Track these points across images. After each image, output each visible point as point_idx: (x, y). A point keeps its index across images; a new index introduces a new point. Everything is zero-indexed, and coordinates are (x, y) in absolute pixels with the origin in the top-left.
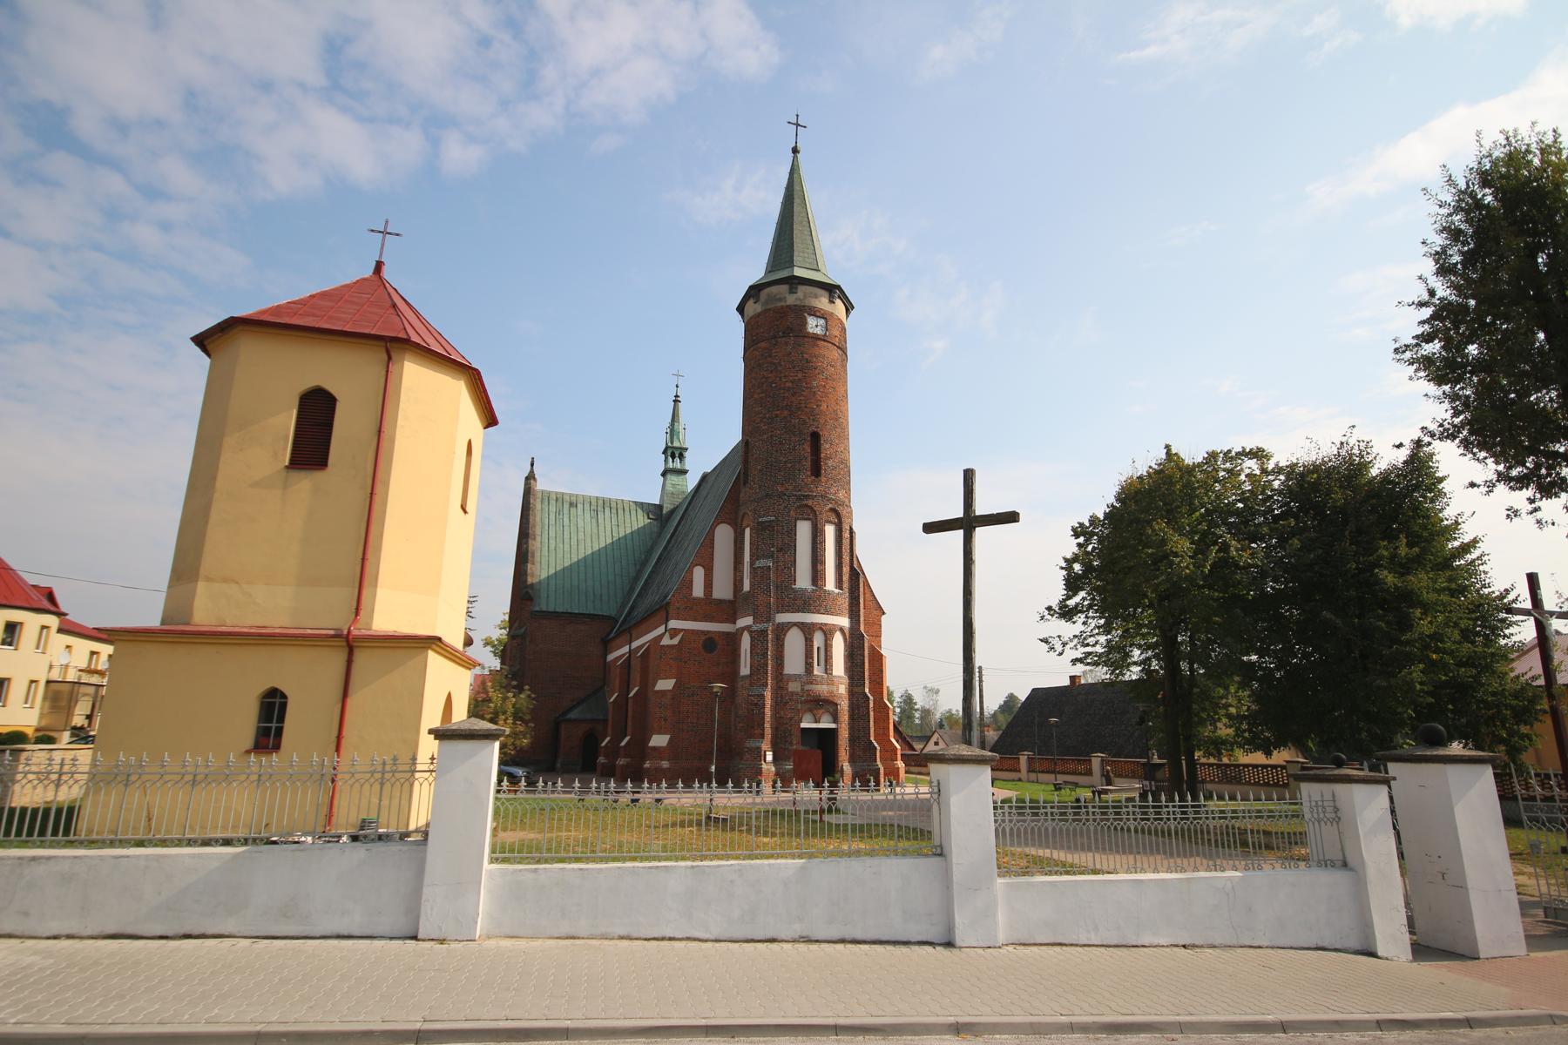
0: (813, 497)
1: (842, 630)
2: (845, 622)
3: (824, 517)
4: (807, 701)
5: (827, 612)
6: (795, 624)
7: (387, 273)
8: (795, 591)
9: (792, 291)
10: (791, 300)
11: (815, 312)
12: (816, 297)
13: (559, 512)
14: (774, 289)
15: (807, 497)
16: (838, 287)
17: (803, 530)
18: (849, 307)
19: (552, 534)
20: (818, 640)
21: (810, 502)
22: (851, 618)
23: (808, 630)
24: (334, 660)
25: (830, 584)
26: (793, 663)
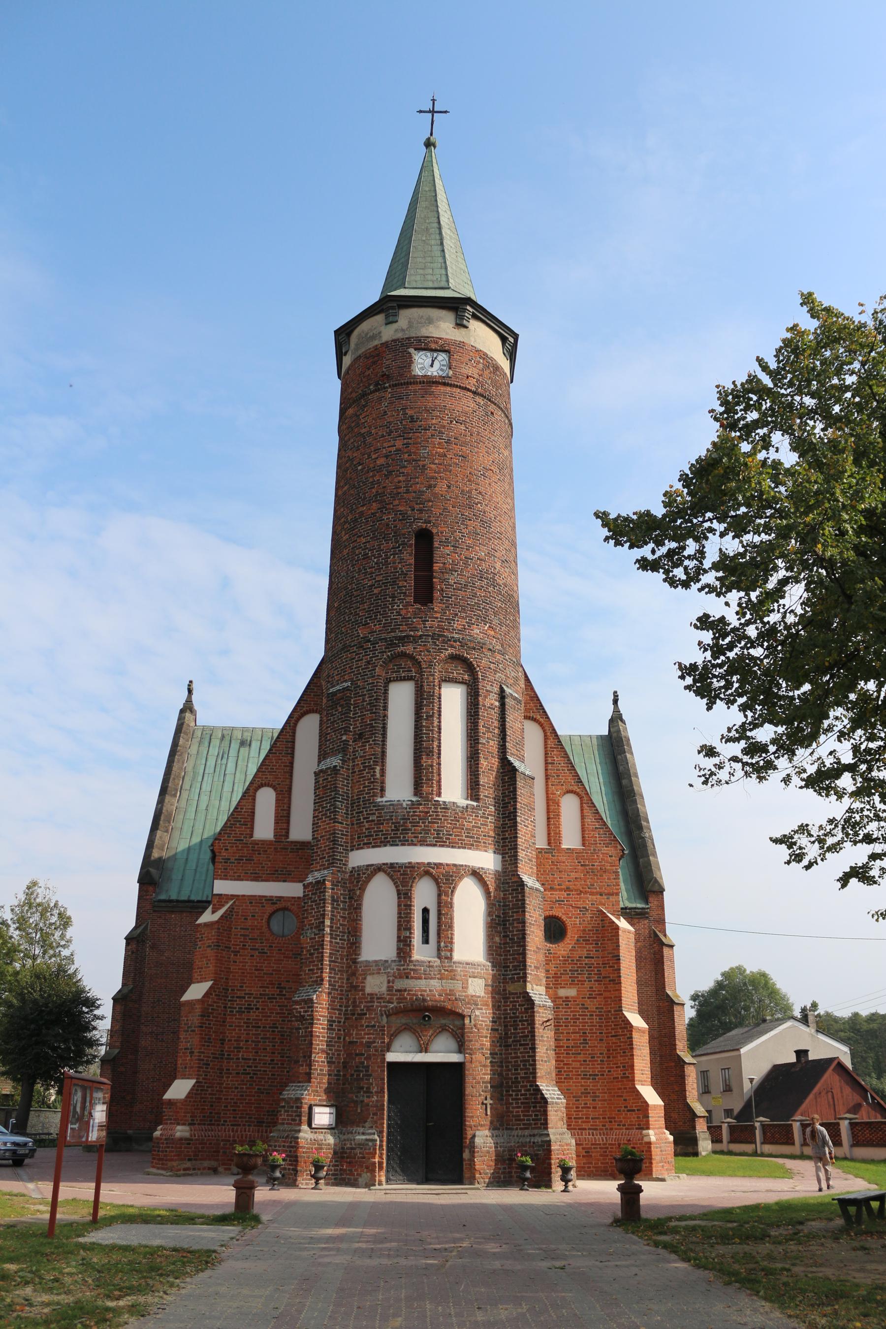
0: (416, 639)
1: (476, 874)
2: (487, 860)
3: (438, 671)
4: (397, 1012)
5: (440, 841)
6: (379, 869)
8: (380, 808)
10: (388, 333)
11: (425, 345)
12: (430, 321)
13: (223, 755)
16: (468, 301)
17: (401, 698)
18: (509, 339)
19: (206, 787)
20: (424, 894)
21: (409, 649)
23: (403, 877)
25: (452, 788)
26: (377, 942)
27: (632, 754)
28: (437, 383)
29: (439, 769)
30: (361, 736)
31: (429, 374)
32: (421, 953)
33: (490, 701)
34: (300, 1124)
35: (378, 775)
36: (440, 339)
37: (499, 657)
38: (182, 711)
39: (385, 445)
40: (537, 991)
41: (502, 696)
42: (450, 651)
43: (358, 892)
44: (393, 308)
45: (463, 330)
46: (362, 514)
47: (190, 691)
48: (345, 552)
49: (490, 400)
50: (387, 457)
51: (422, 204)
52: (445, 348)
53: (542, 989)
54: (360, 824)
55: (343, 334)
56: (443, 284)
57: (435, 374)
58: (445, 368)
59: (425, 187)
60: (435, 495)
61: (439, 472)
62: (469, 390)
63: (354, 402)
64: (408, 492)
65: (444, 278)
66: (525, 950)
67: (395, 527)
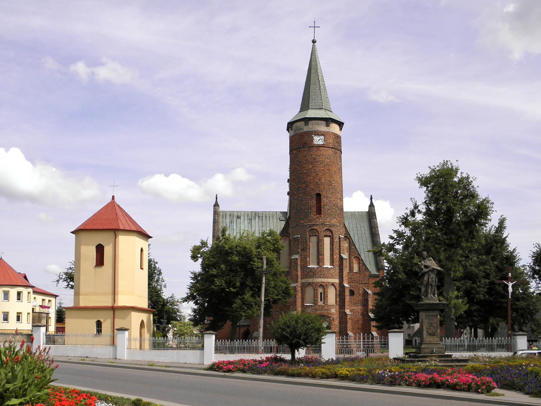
0: (317, 225)
1: (333, 284)
7: (116, 200)
9: (306, 124)
10: (306, 129)
11: (318, 134)
13: (231, 222)
14: (298, 124)
15: (314, 225)
18: (341, 124)
20: (320, 290)
21: (315, 228)
22: (339, 279)
24: (112, 312)
25: (327, 265)
28: (321, 147)
30: (303, 250)
32: (320, 303)
33: (337, 240)
38: (214, 206)
40: (348, 311)
46: (300, 187)
47: (217, 198)
51: (313, 71)
53: (349, 310)
55: (290, 125)
56: (321, 107)
59: (313, 64)
60: (321, 183)
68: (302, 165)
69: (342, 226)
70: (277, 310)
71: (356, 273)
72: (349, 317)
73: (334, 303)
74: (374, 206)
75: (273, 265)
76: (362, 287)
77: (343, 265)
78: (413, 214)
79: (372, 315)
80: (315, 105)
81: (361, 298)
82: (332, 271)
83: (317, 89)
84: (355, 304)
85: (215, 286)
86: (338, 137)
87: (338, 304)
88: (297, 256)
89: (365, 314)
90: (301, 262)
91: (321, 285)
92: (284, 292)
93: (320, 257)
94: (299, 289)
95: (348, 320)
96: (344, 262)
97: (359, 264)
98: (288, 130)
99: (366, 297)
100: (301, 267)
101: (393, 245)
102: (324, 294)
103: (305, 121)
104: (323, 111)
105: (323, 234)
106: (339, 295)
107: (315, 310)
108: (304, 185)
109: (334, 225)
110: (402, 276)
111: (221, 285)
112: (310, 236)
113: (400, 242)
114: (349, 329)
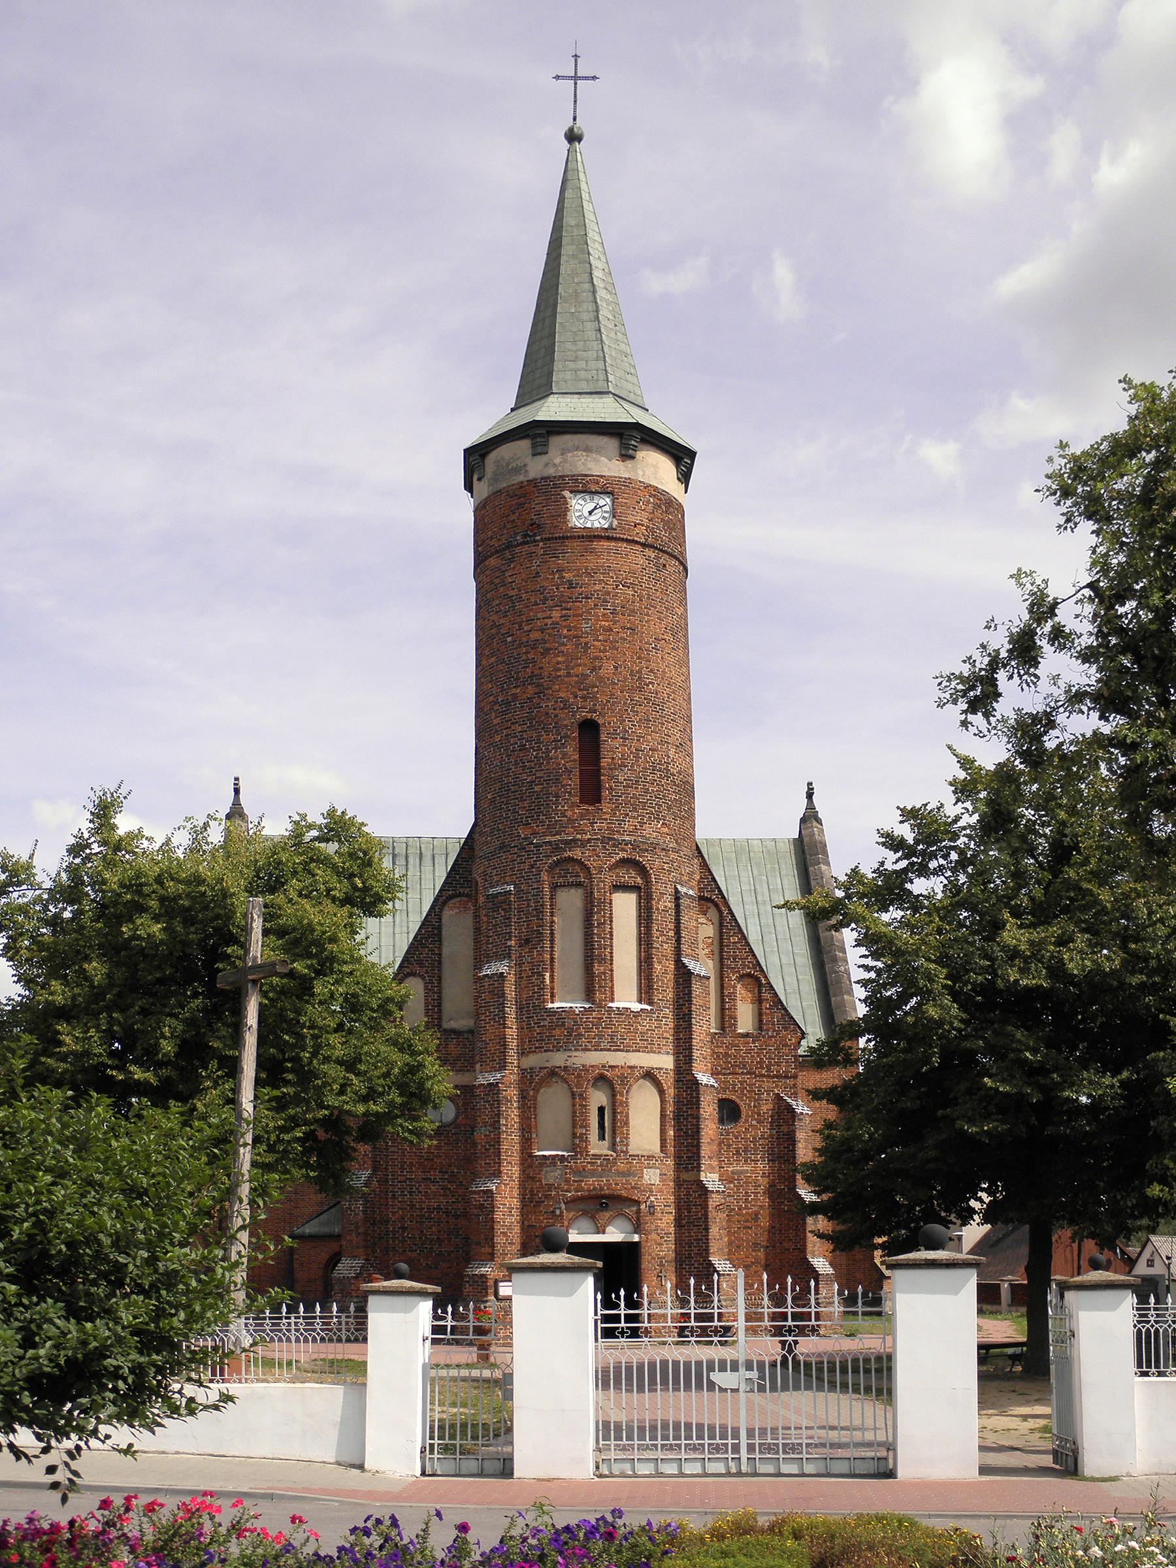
0: (584, 844)
4: (575, 1200)
9: (539, 450)
10: (536, 468)
11: (586, 486)
14: (504, 452)
18: (683, 458)
20: (598, 1098)
21: (577, 854)
22: (677, 1054)
25: (626, 997)
27: (828, 864)
28: (599, 538)
29: (612, 976)
30: (527, 941)
31: (588, 525)
32: (598, 1147)
34: (487, 1294)
35: (548, 982)
36: (601, 476)
37: (673, 856)
39: (539, 615)
40: (711, 1179)
41: (677, 896)
42: (621, 855)
43: (531, 1093)
44: (540, 435)
45: (629, 463)
46: (515, 696)
47: (237, 791)
48: (497, 738)
49: (661, 550)
50: (542, 631)
51: (567, 250)
52: (605, 487)
53: (715, 1176)
54: (530, 1028)
56: (601, 386)
57: (597, 525)
58: (606, 515)
59: (569, 220)
60: (601, 679)
61: (605, 651)
62: (637, 542)
63: (497, 552)
64: (569, 675)
65: (602, 377)
66: (699, 1143)
67: (556, 716)
68: (521, 613)
69: (685, 851)
70: (432, 1175)
71: (747, 1035)
72: (714, 1201)
73: (656, 1147)
74: (819, 822)
75: (332, 959)
76: (769, 1089)
77: (690, 1001)
78: (1024, 650)
79: (807, 1194)
80: (578, 380)
81: (765, 1130)
82: (645, 1024)
83: (585, 316)
84: (741, 1153)
85: (63, 1058)
86: (670, 510)
87: (671, 1149)
88: (502, 967)
89: (781, 1192)
90: (519, 989)
91: (602, 1077)
92: (402, 1087)
93: (597, 968)
94: (512, 1093)
95: (712, 1213)
96: (696, 988)
97: (759, 1001)
98: (469, 486)
99: (785, 1129)
100: (520, 1009)
101: (902, 876)
102: (614, 1112)
103: (533, 437)
104: (609, 399)
105: (609, 879)
106: (677, 1117)
107: (576, 1172)
108: (531, 689)
109: (654, 846)
110: (944, 1010)
111: (87, 1054)
112: (555, 887)
113: (933, 864)
114: (714, 1246)
